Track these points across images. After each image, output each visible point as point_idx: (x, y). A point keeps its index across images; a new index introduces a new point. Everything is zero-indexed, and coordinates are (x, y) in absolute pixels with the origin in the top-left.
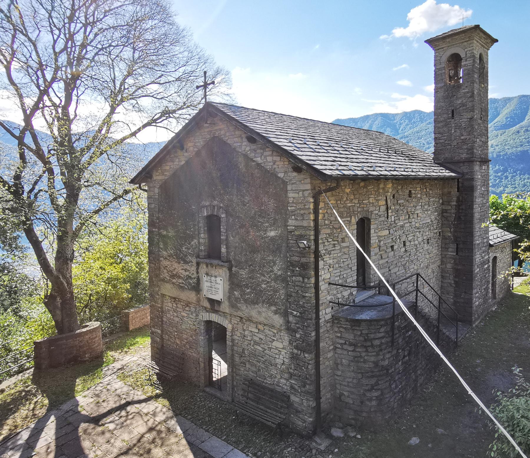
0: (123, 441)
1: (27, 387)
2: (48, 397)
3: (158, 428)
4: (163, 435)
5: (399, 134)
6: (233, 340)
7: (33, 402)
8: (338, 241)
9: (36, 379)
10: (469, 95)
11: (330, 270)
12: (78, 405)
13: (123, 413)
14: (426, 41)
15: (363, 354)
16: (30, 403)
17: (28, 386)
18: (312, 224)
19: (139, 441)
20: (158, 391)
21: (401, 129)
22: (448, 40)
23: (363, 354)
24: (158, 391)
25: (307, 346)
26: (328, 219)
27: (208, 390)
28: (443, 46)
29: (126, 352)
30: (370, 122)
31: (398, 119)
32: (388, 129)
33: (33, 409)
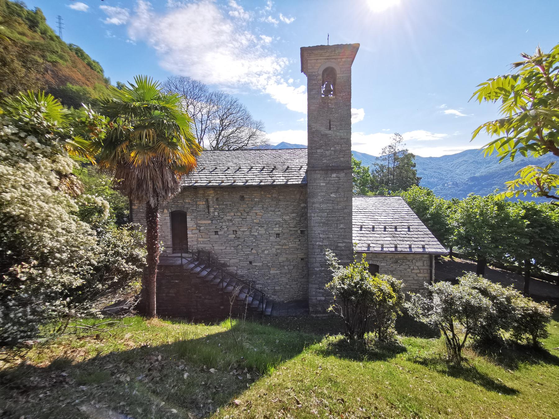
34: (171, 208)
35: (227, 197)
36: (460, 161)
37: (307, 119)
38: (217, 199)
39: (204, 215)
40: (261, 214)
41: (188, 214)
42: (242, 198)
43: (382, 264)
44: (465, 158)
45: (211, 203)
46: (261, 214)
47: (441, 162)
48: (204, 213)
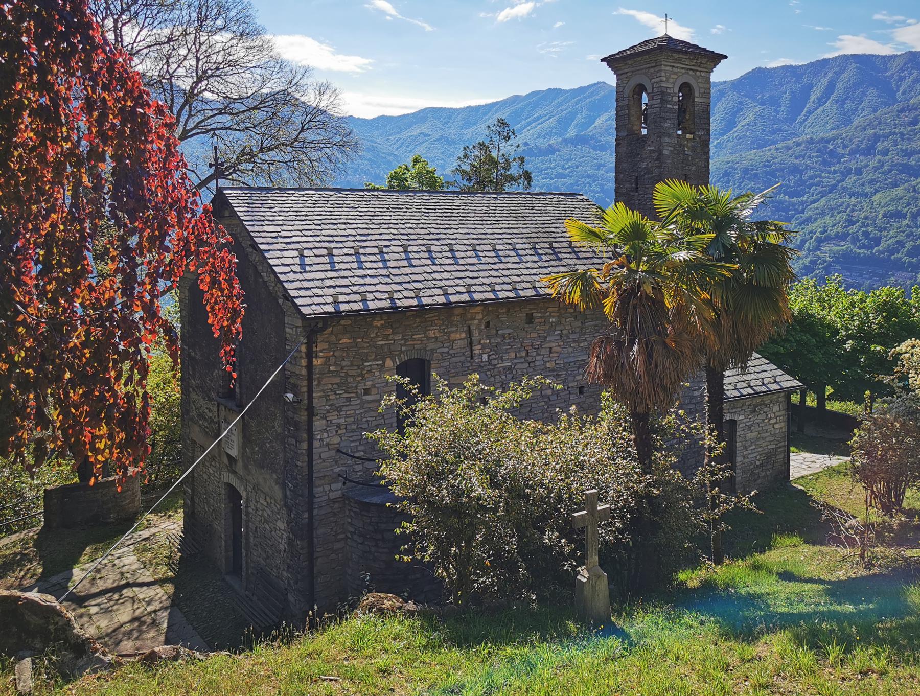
0: (98, 627)
1: (26, 549)
2: (44, 566)
3: (143, 619)
4: (144, 628)
5: (896, 101)
6: (248, 514)
7: (25, 569)
8: (356, 393)
9: (39, 542)
10: (655, 155)
11: (340, 432)
12: (70, 579)
13: (116, 597)
14: (603, 60)
15: (373, 549)
16: (21, 570)
17: (28, 548)
18: (304, 372)
19: (114, 631)
20: (170, 574)
21: (901, 90)
22: (630, 62)
23: (373, 549)
24: (170, 574)
25: (304, 531)
26: (335, 364)
27: (228, 578)
28: (626, 71)
29: (170, 516)
30: (830, 75)
31: (894, 67)
32: (871, 90)
33: (21, 579)
34: (399, 355)
35: (504, 318)
36: (414, 133)
37: (610, 159)
38: (488, 325)
39: (463, 363)
40: (558, 349)
41: (434, 364)
42: (530, 319)
43: (741, 418)
44: (424, 128)
45: (476, 333)
46: (558, 349)
47: (376, 133)
48: (462, 358)
